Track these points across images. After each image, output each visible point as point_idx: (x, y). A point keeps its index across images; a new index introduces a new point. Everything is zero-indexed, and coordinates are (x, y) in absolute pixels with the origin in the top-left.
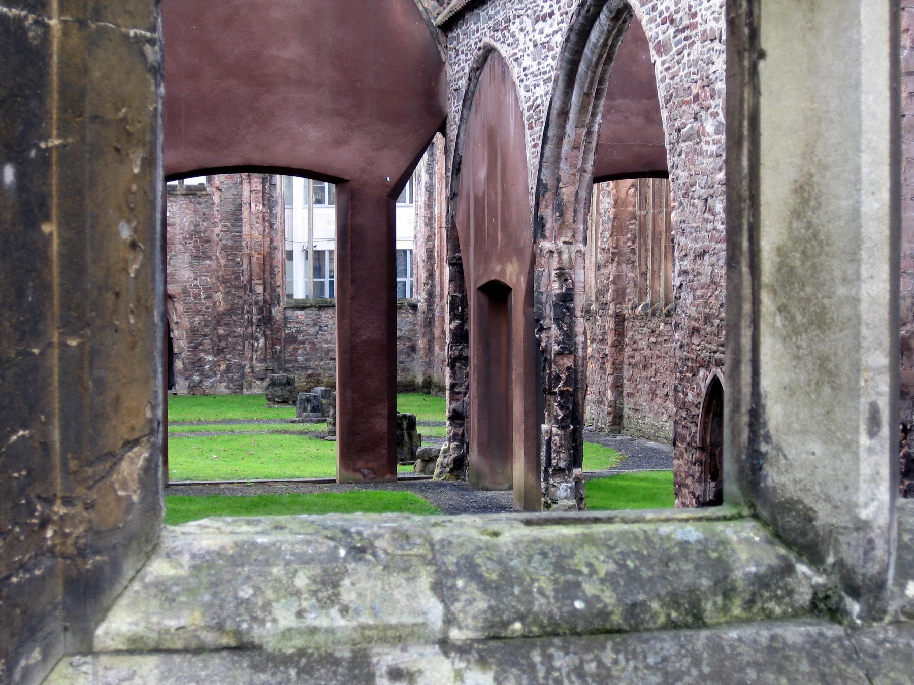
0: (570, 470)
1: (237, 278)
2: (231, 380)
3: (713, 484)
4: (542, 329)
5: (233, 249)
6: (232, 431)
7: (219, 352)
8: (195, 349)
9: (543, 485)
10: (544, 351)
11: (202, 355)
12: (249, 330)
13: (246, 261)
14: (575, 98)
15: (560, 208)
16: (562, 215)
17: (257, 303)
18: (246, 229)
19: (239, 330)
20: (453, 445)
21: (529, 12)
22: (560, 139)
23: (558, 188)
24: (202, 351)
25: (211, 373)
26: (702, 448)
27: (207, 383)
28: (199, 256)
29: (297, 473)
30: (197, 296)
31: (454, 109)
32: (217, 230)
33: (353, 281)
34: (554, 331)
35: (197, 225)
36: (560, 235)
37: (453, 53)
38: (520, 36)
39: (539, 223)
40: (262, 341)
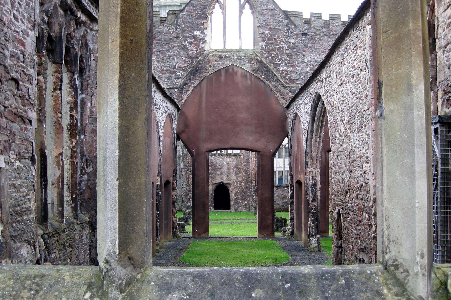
0: (316, 235)
1: (248, 179)
2: (246, 207)
3: (340, 241)
4: (307, 194)
5: (247, 171)
6: (240, 222)
7: (243, 199)
8: (236, 199)
9: (308, 240)
10: (308, 200)
11: (238, 200)
12: (251, 193)
13: (250, 174)
14: (315, 127)
15: (312, 159)
16: (313, 161)
17: (253, 186)
18: (250, 165)
19: (249, 193)
20: (291, 227)
21: (304, 103)
22: (312, 139)
23: (311, 153)
24: (238, 199)
25: (241, 206)
26: (337, 230)
27: (239, 208)
28: (237, 173)
29: (250, 235)
30: (237, 184)
31: (290, 130)
32: (242, 165)
33: (262, 180)
34: (311, 195)
35: (237, 164)
36: (312, 167)
37: (289, 115)
38: (302, 109)
39: (306, 163)
40: (255, 196)
